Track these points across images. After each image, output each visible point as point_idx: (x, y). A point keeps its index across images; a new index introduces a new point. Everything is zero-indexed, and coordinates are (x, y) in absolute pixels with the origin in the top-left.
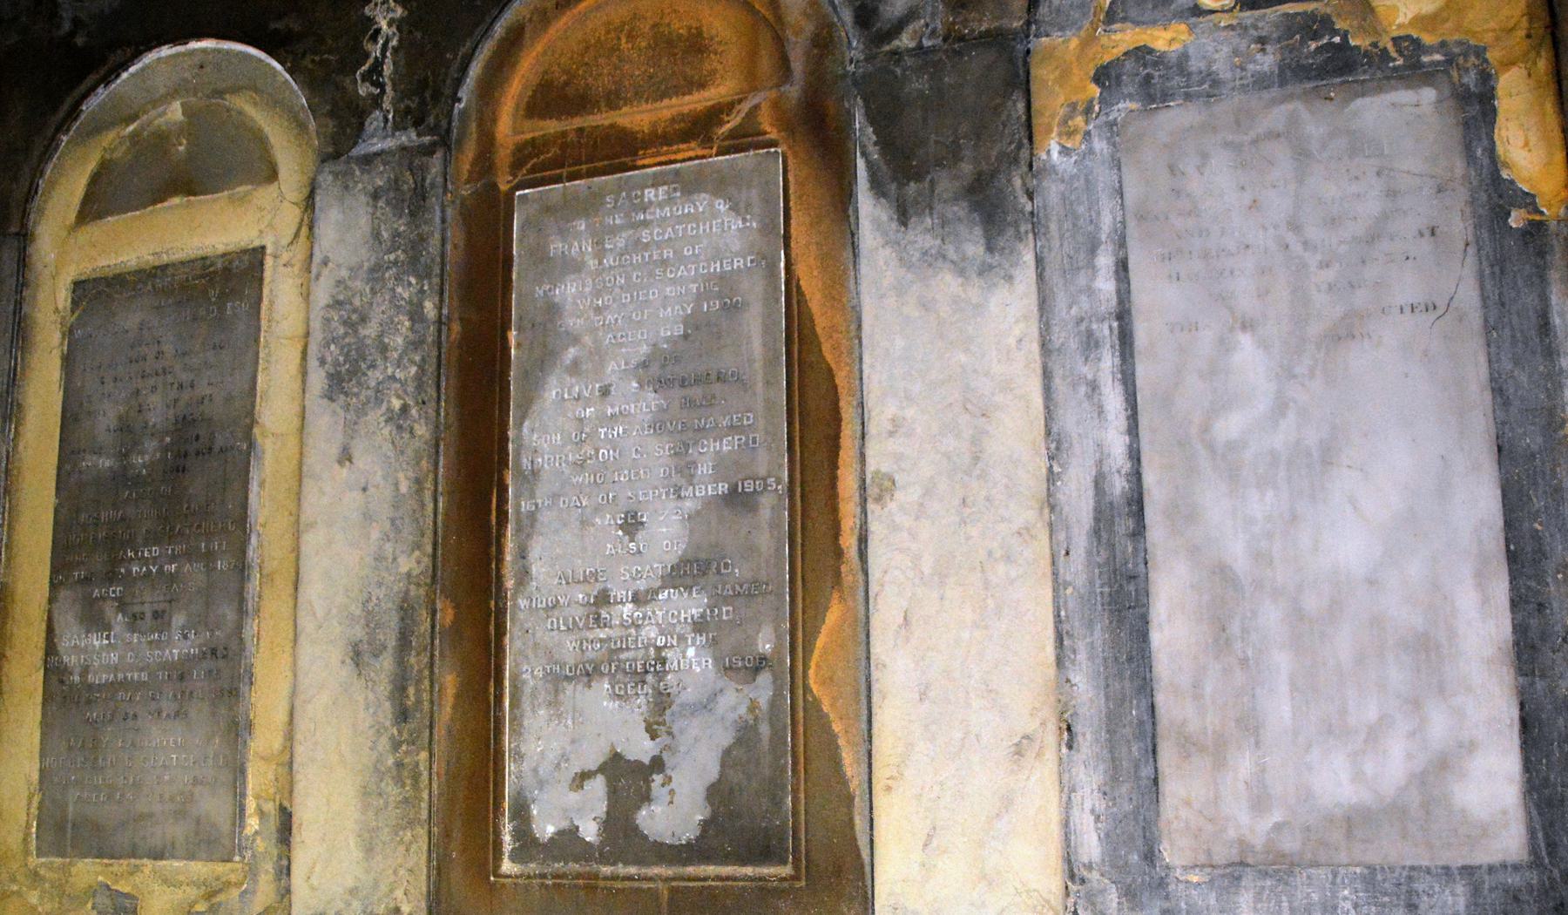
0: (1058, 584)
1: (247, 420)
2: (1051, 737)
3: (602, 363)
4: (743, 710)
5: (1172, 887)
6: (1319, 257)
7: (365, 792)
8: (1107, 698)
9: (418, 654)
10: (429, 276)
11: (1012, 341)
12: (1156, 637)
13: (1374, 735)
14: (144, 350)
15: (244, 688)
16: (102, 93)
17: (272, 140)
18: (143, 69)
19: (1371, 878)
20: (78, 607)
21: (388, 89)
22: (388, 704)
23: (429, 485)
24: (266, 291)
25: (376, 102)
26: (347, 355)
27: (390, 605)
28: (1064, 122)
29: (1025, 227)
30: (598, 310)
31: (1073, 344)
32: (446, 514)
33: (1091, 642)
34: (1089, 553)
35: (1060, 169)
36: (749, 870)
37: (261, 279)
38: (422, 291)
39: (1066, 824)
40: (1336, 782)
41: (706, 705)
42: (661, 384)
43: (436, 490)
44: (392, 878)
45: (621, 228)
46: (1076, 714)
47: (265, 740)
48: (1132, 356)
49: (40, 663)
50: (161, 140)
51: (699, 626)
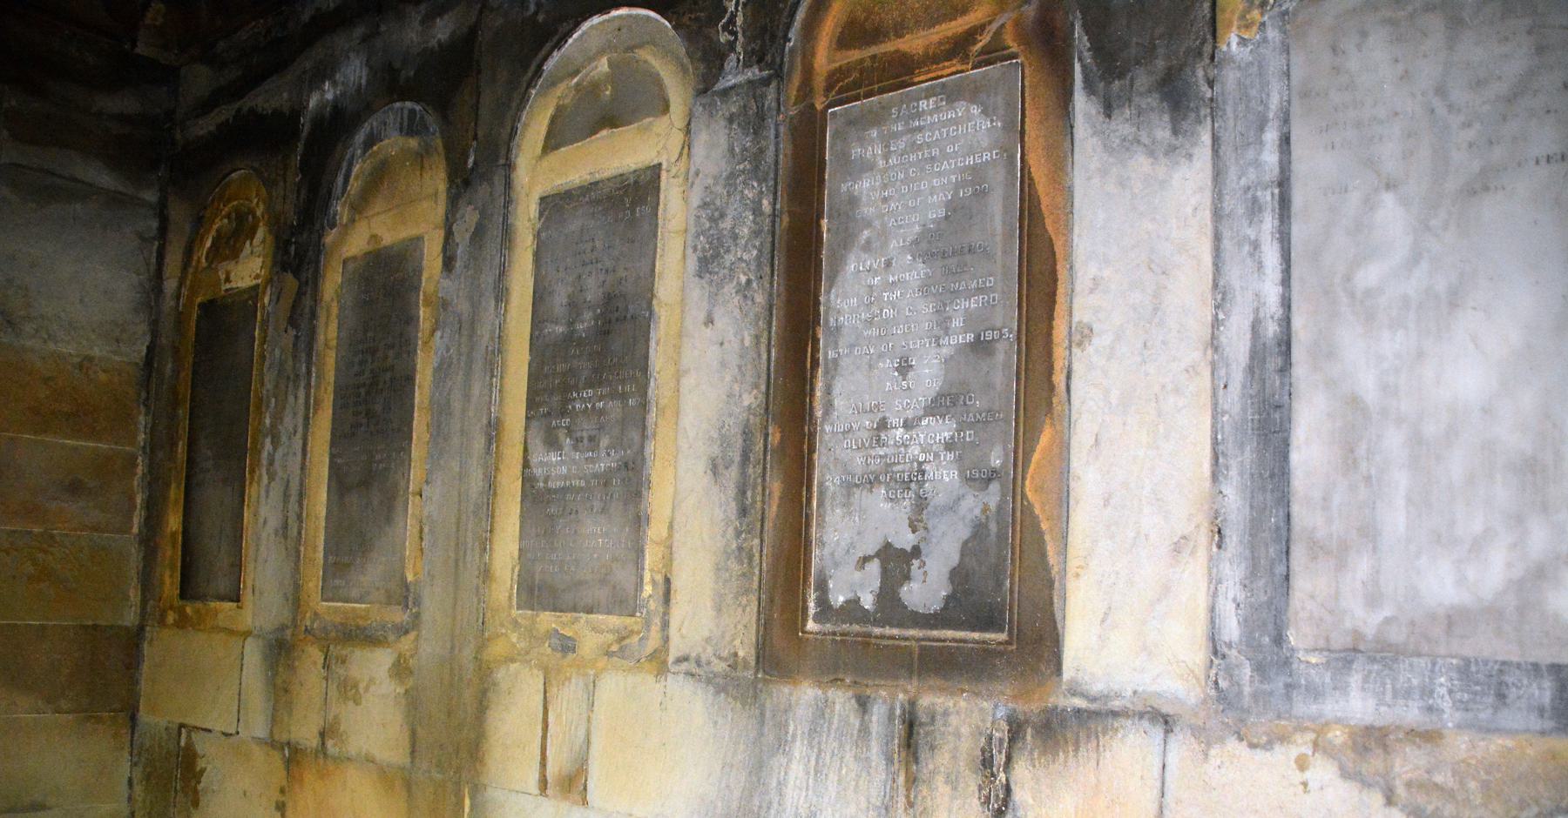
0: (1216, 413)
1: (648, 295)
2: (1203, 538)
3: (885, 244)
4: (977, 512)
5: (1295, 666)
6: (1462, 118)
8: (1252, 507)
10: (765, 180)
11: (1189, 210)
12: (1295, 457)
13: (1478, 546)
16: (556, 55)
18: (581, 36)
19: (1465, 670)
21: (740, 36)
22: (733, 504)
23: (764, 340)
25: (731, 46)
28: (1243, 17)
29: (1205, 111)
30: (885, 200)
31: (1241, 211)
33: (1241, 461)
34: (1244, 387)
35: (1238, 58)
36: (976, 635)
39: (1212, 609)
40: (1442, 585)
41: (952, 507)
42: (928, 256)
45: (902, 134)
46: (1225, 520)
47: (655, 531)
48: (1289, 217)
50: (594, 88)
51: (949, 446)
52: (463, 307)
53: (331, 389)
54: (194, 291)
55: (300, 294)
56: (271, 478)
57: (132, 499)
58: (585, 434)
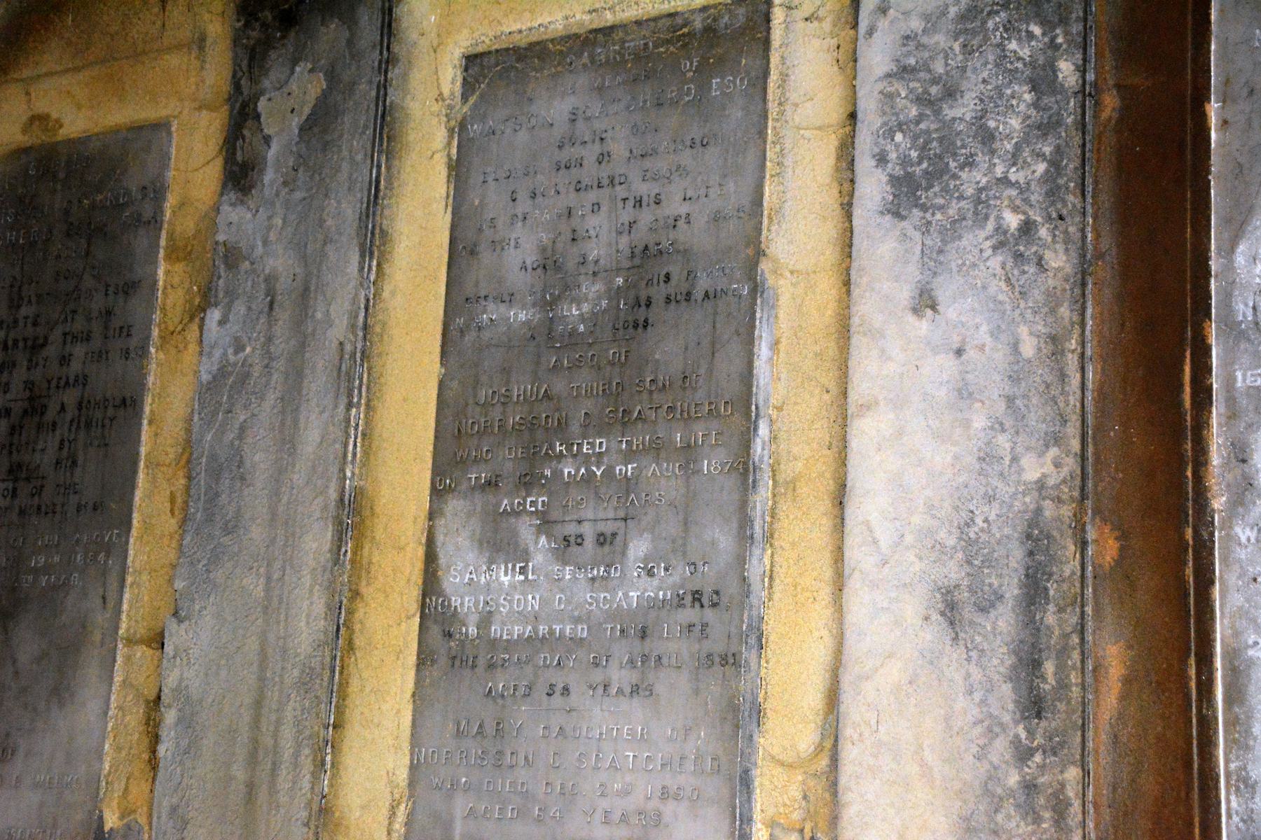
9: (1061, 610)
10: (1064, 21)
15: (749, 655)
22: (1007, 689)
26: (924, 148)
27: (1007, 531)
37: (767, 43)
38: (1053, 45)
47: (788, 731)
49: (414, 607)
52: (280, 262)
58: (588, 530)
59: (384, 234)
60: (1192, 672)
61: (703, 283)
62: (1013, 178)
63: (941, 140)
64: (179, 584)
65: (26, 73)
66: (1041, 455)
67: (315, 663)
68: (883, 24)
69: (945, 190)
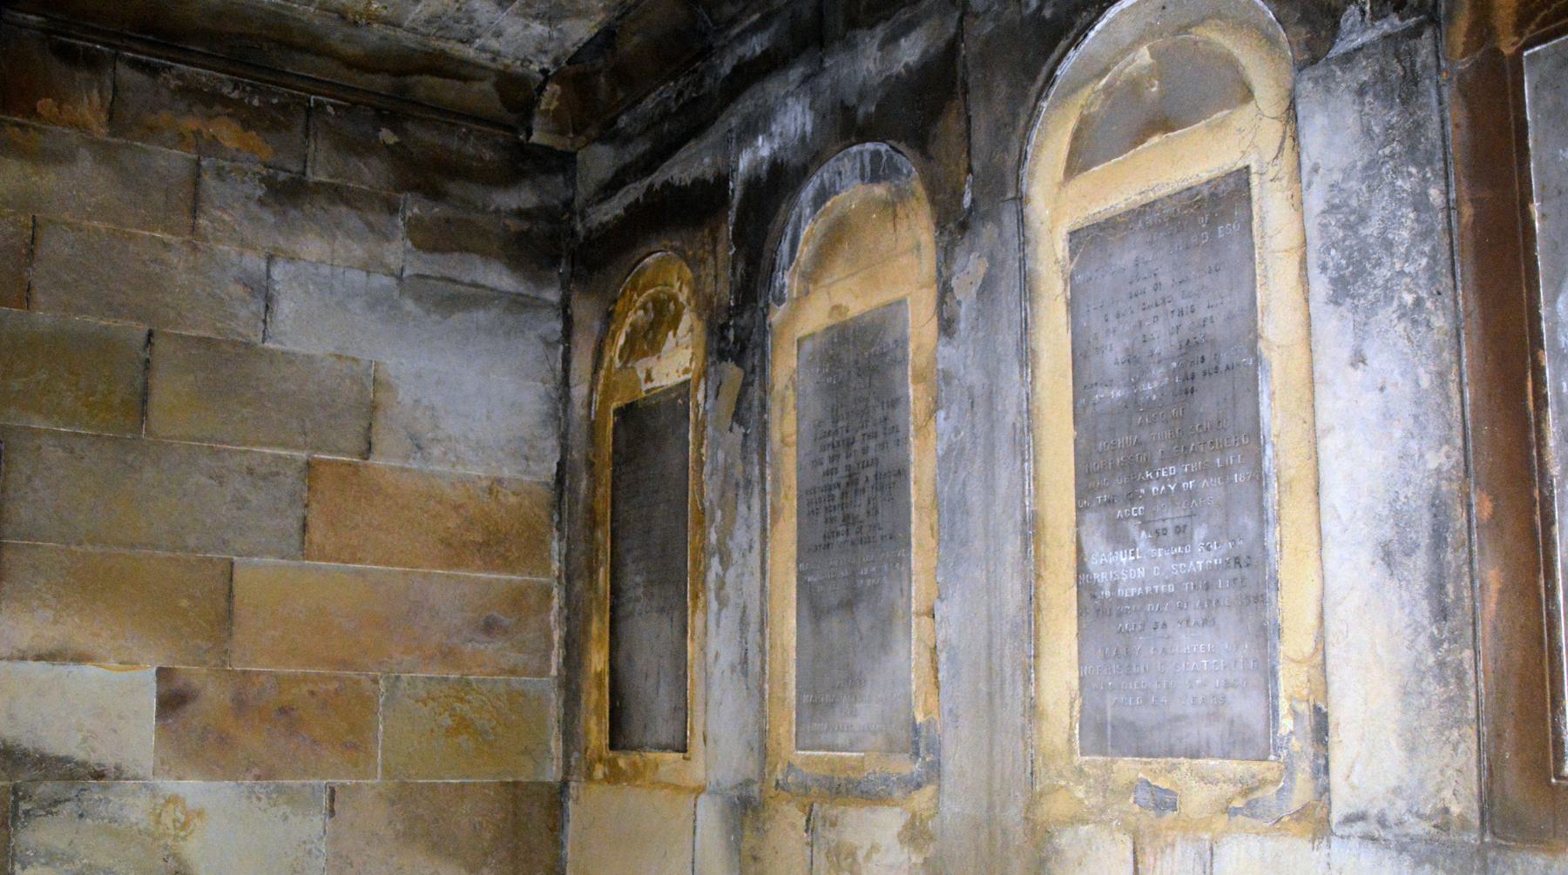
1: (1252, 337)
7: (1405, 693)
9: (1456, 550)
10: (1430, 162)
14: (1141, 284)
15: (1270, 594)
17: (1243, 61)
18: (1108, 25)
20: (1103, 527)
22: (1424, 604)
23: (1453, 376)
24: (1255, 209)
26: (1350, 257)
27: (1420, 502)
32: (1474, 404)
37: (1249, 199)
38: (1425, 179)
43: (1461, 382)
44: (1439, 778)
47: (1295, 643)
49: (1073, 581)
50: (1135, 85)
52: (975, 378)
53: (793, 493)
54: (607, 396)
55: (746, 385)
56: (722, 603)
57: (548, 636)
58: (1169, 524)
59: (1033, 351)
60: (1542, 583)
61: (1225, 359)
62: (1407, 270)
63: (1359, 250)
64: (939, 579)
65: (827, 281)
66: (1438, 450)
67: (1018, 620)
68: (1317, 179)
69: (1365, 283)
